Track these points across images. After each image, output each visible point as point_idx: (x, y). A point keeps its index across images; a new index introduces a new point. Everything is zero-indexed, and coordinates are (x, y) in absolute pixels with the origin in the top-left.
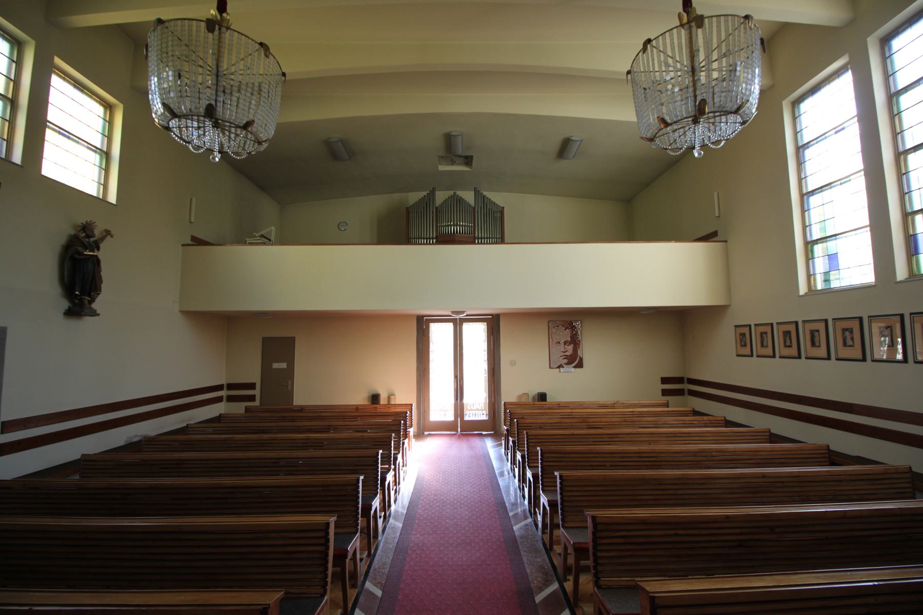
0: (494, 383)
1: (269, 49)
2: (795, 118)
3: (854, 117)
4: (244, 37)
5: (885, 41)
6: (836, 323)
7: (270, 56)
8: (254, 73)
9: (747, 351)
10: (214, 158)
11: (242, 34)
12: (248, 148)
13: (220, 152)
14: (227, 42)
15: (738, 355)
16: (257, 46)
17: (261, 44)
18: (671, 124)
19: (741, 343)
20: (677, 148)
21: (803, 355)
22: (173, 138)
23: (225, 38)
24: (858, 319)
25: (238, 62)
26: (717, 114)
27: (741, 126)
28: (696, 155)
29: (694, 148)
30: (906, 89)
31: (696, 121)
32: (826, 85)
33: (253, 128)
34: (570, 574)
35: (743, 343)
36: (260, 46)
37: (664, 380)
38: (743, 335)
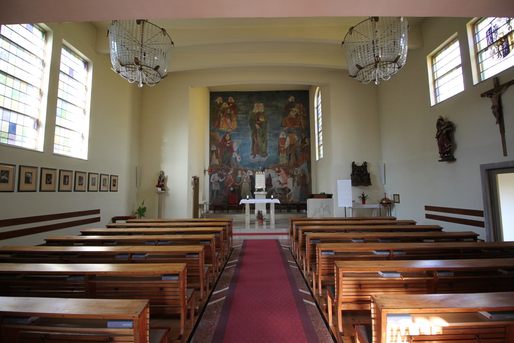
0: (359, 258)
1: (166, 31)
2: (474, 35)
3: (457, 67)
4: (154, 26)
5: (433, 57)
6: (70, 189)
7: (166, 34)
8: (159, 43)
9: (113, 178)
10: (140, 86)
11: (153, 24)
12: (156, 80)
13: (143, 83)
14: (146, 28)
15: (117, 176)
16: (160, 30)
17: (162, 29)
18: (364, 68)
19: (95, 180)
20: (367, 81)
21: (110, 176)
22: (123, 78)
23: (146, 26)
24: (60, 190)
25: (152, 38)
26: (388, 63)
27: (398, 69)
28: (376, 83)
29: (375, 80)
30: (457, 67)
31: (376, 67)
32: (452, 44)
33: (159, 70)
34: (241, 162)
35: (94, 180)
36: (162, 30)
37: (427, 208)
38: (114, 185)
